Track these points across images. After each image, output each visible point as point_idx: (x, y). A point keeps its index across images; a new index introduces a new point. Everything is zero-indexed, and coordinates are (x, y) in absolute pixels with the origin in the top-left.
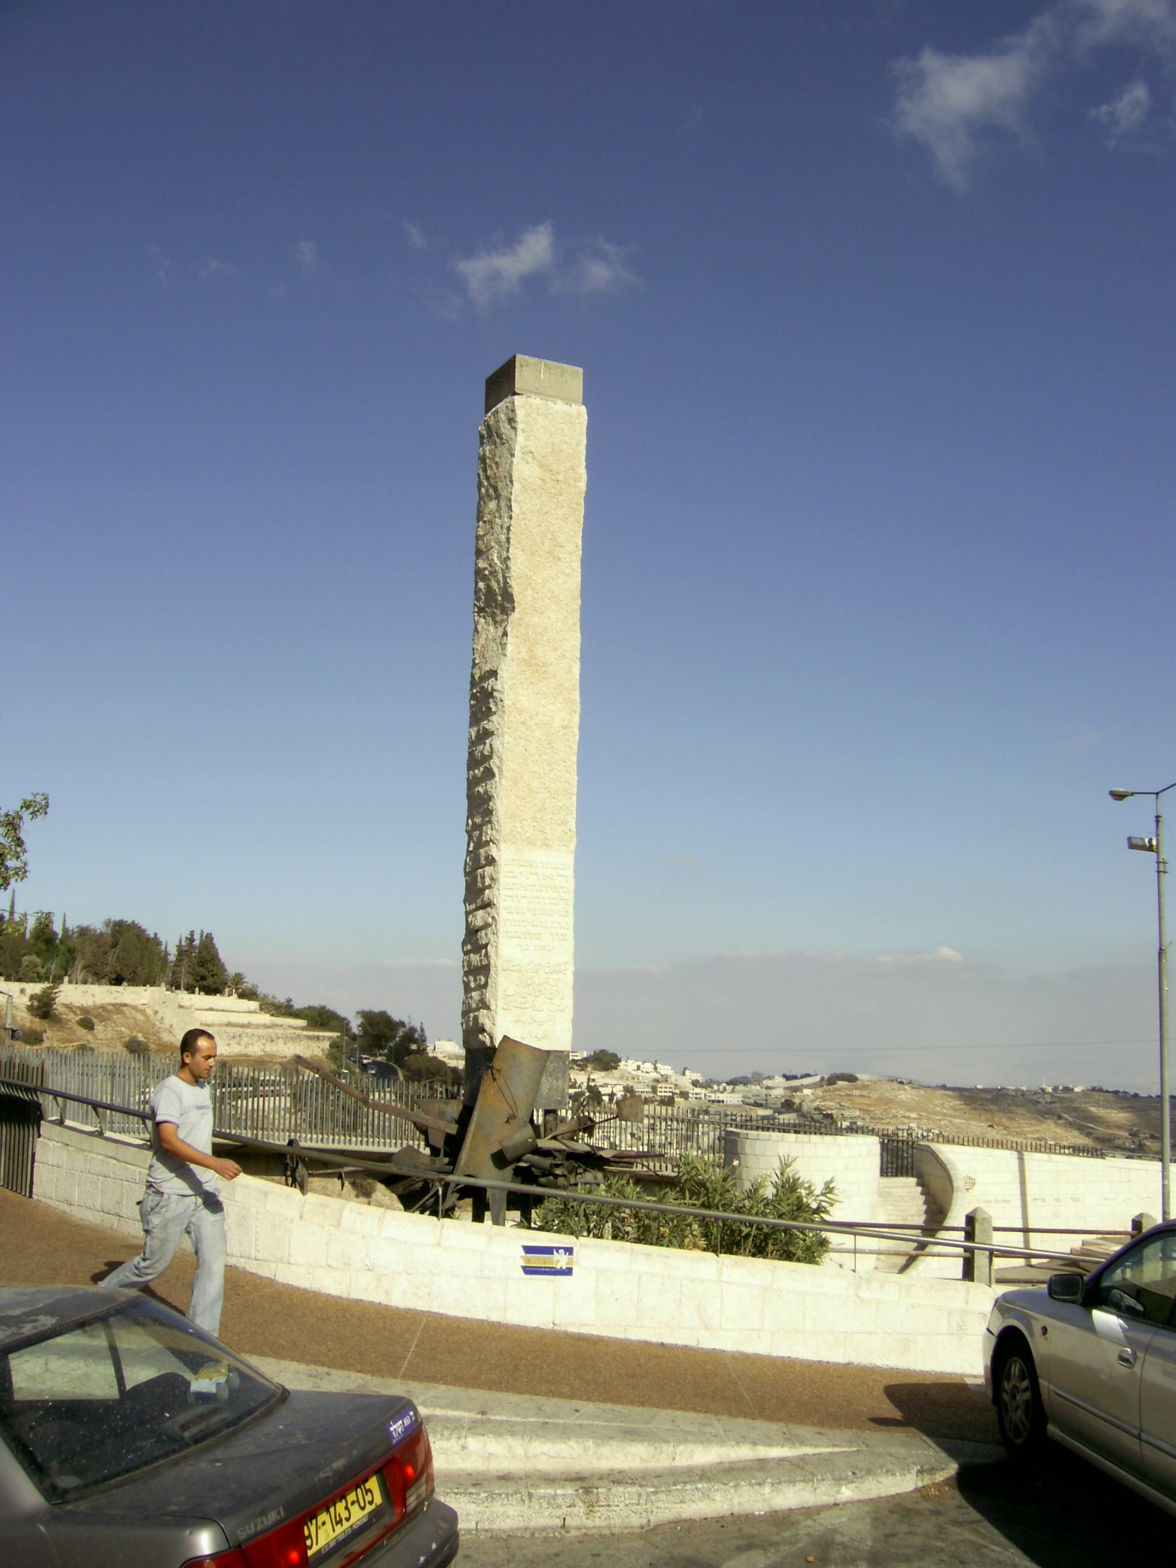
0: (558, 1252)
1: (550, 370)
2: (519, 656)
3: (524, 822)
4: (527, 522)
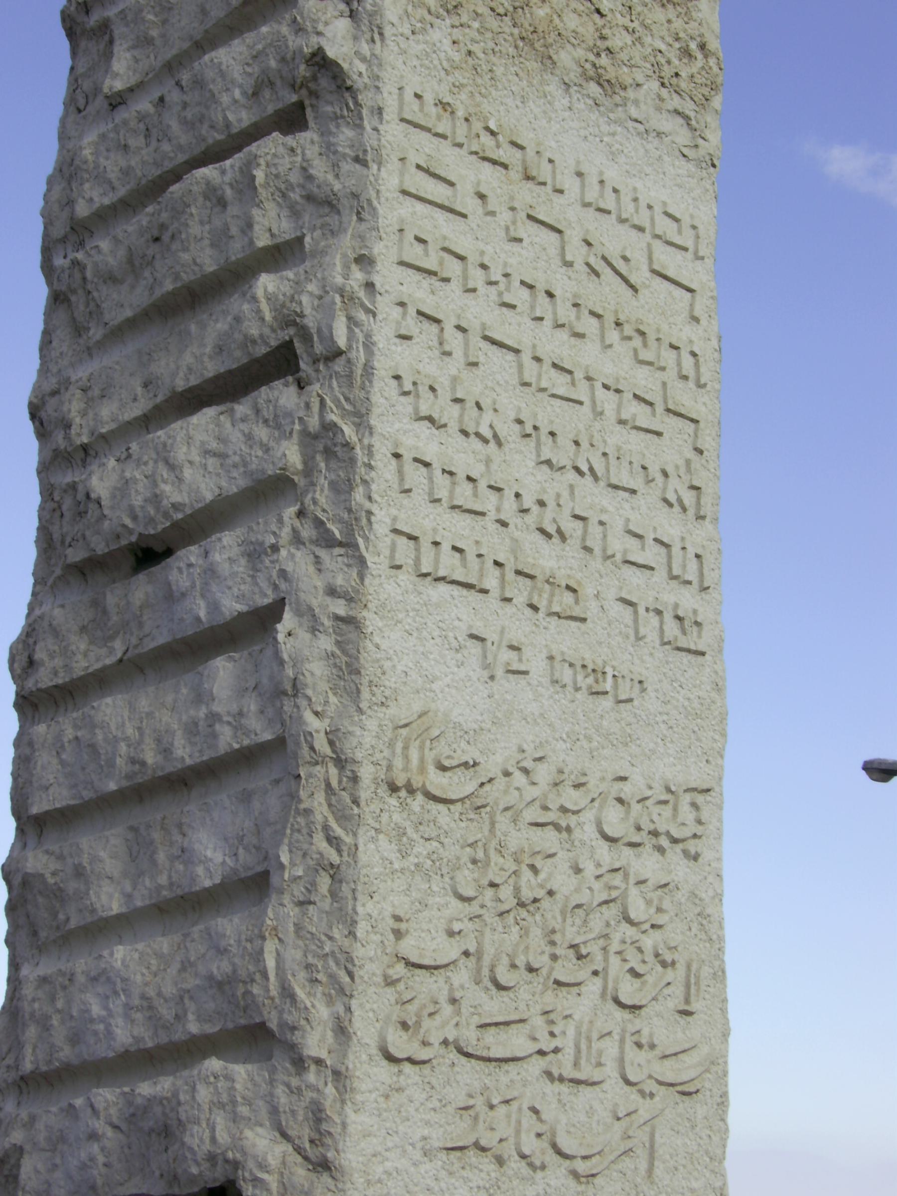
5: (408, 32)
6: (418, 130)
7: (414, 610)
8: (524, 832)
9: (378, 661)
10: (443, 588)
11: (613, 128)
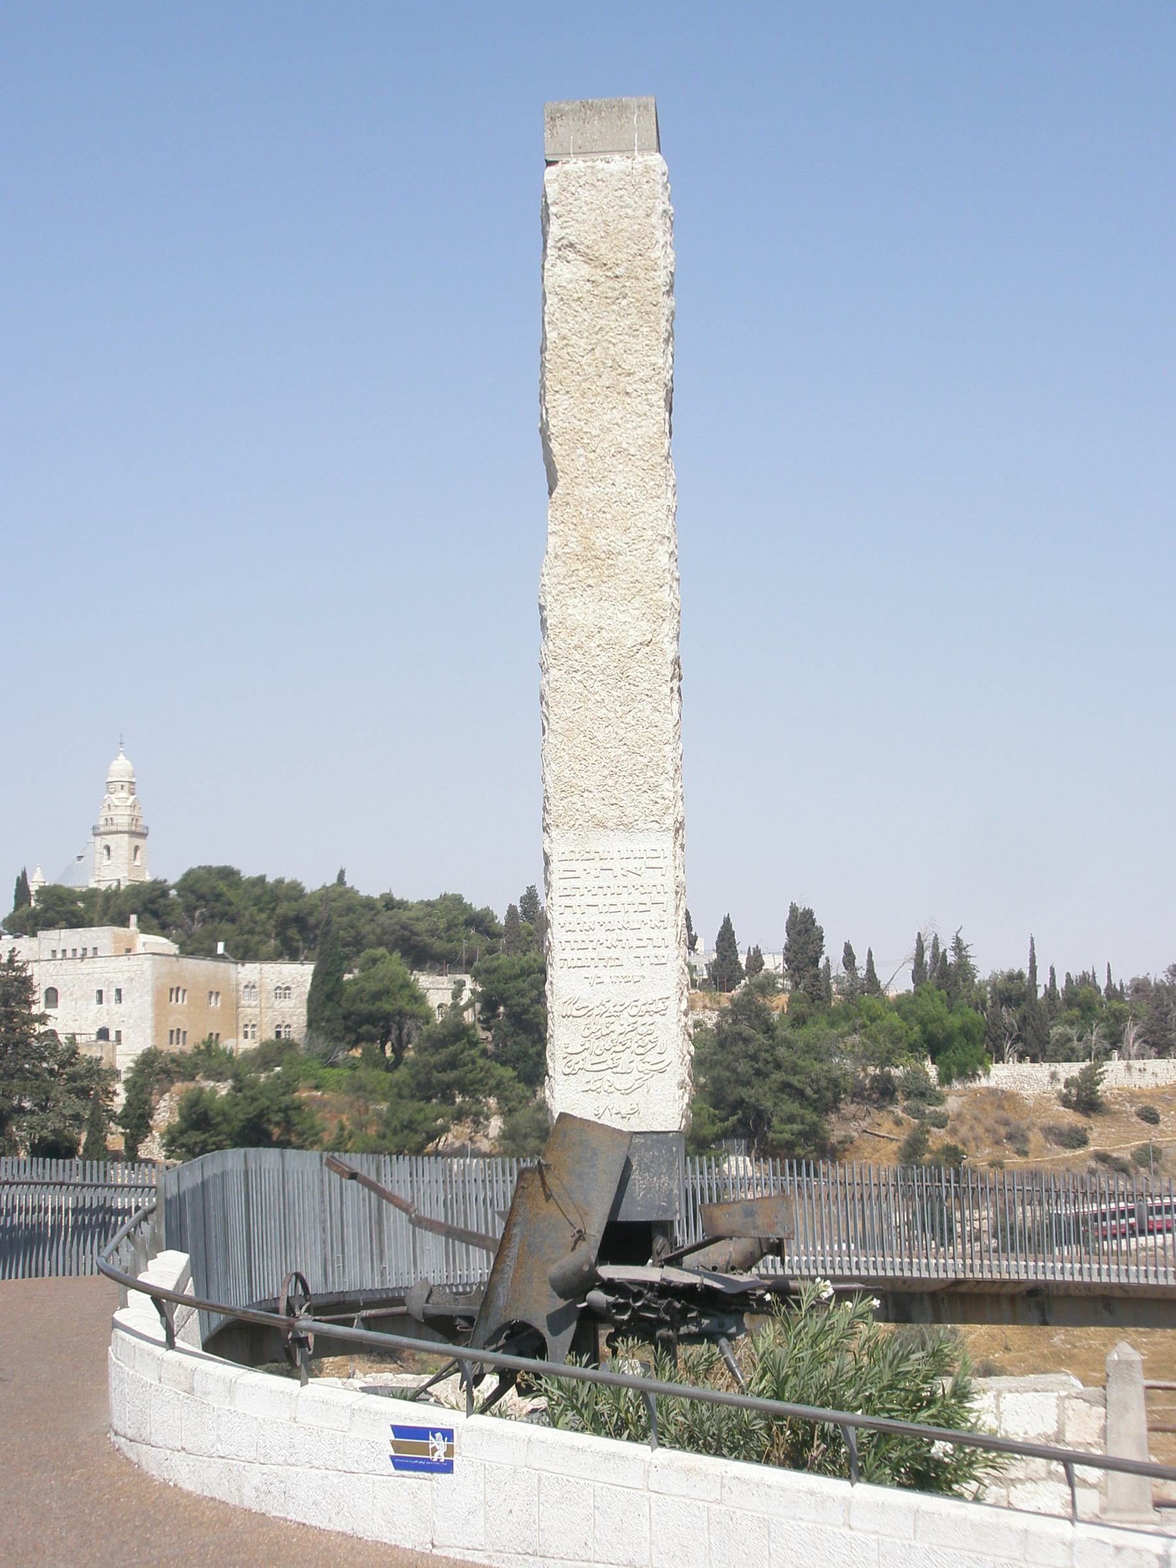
0: (434, 1437)
1: (600, 112)
2: (567, 550)
3: (585, 794)
4: (570, 349)
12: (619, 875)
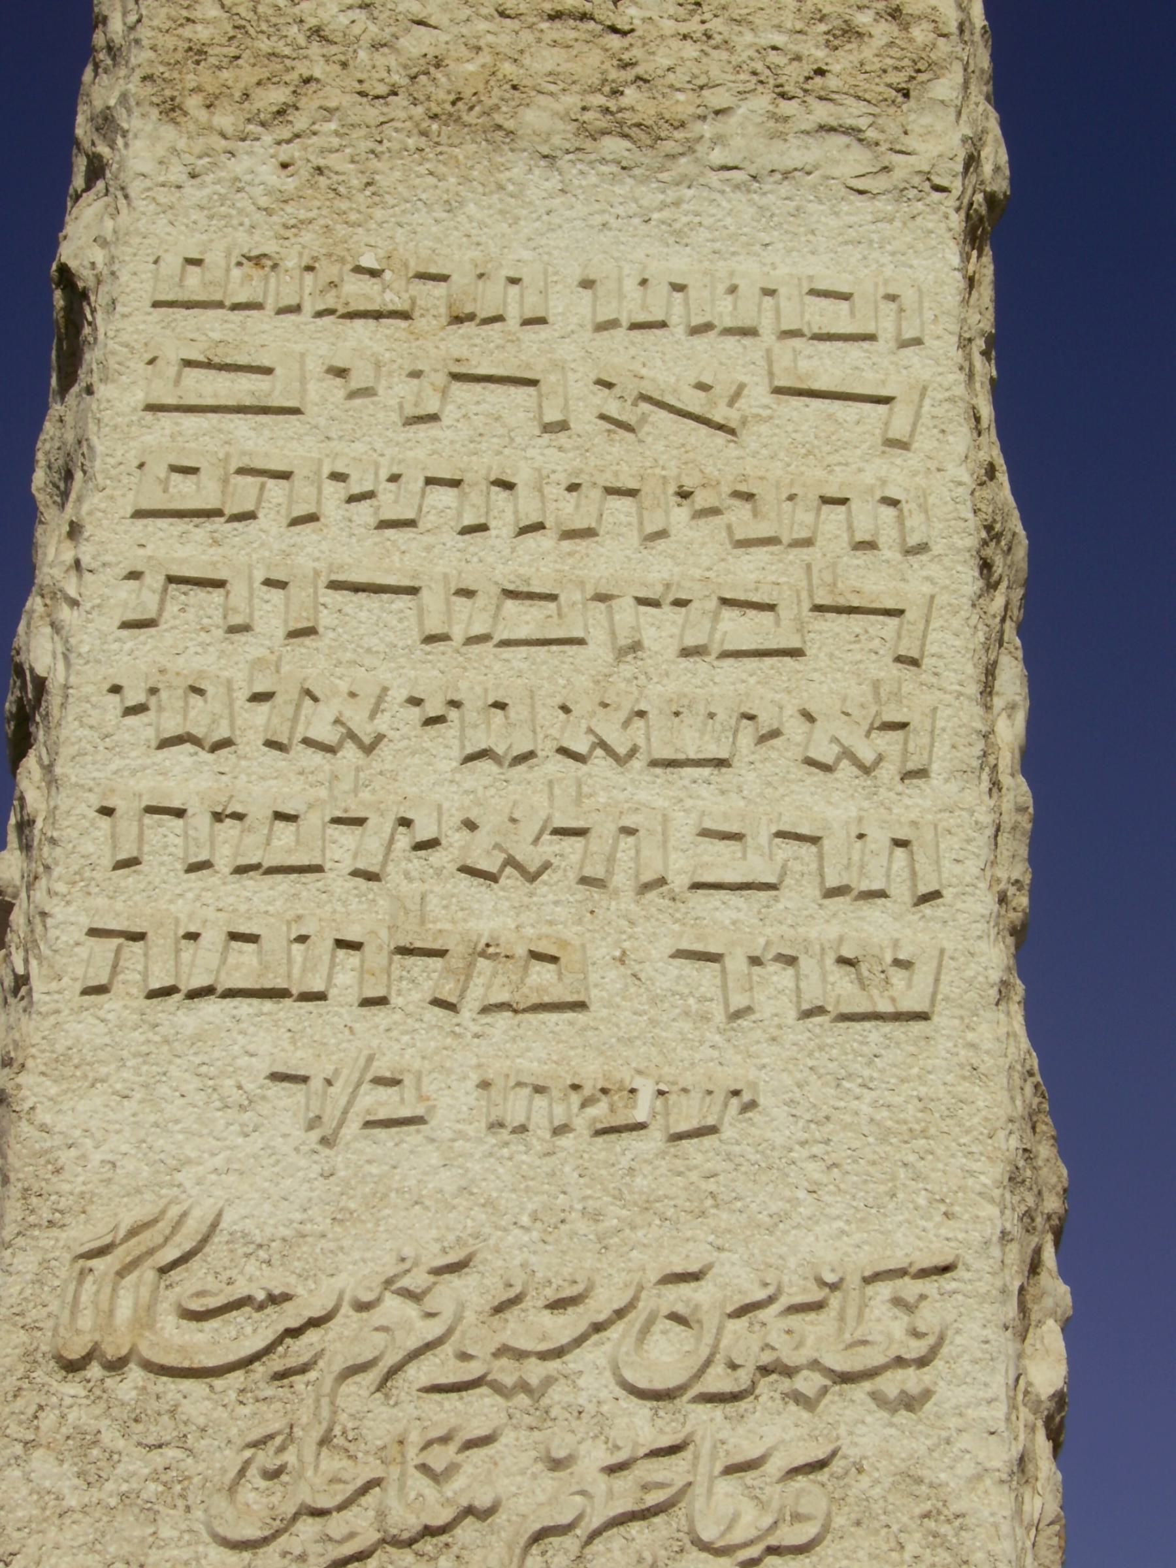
5: (183, 178)
6: (196, 311)
7: (136, 1055)
8: (410, 1408)
9: (44, 1153)
10: (210, 1007)
11: (672, 194)
12: (584, 421)
